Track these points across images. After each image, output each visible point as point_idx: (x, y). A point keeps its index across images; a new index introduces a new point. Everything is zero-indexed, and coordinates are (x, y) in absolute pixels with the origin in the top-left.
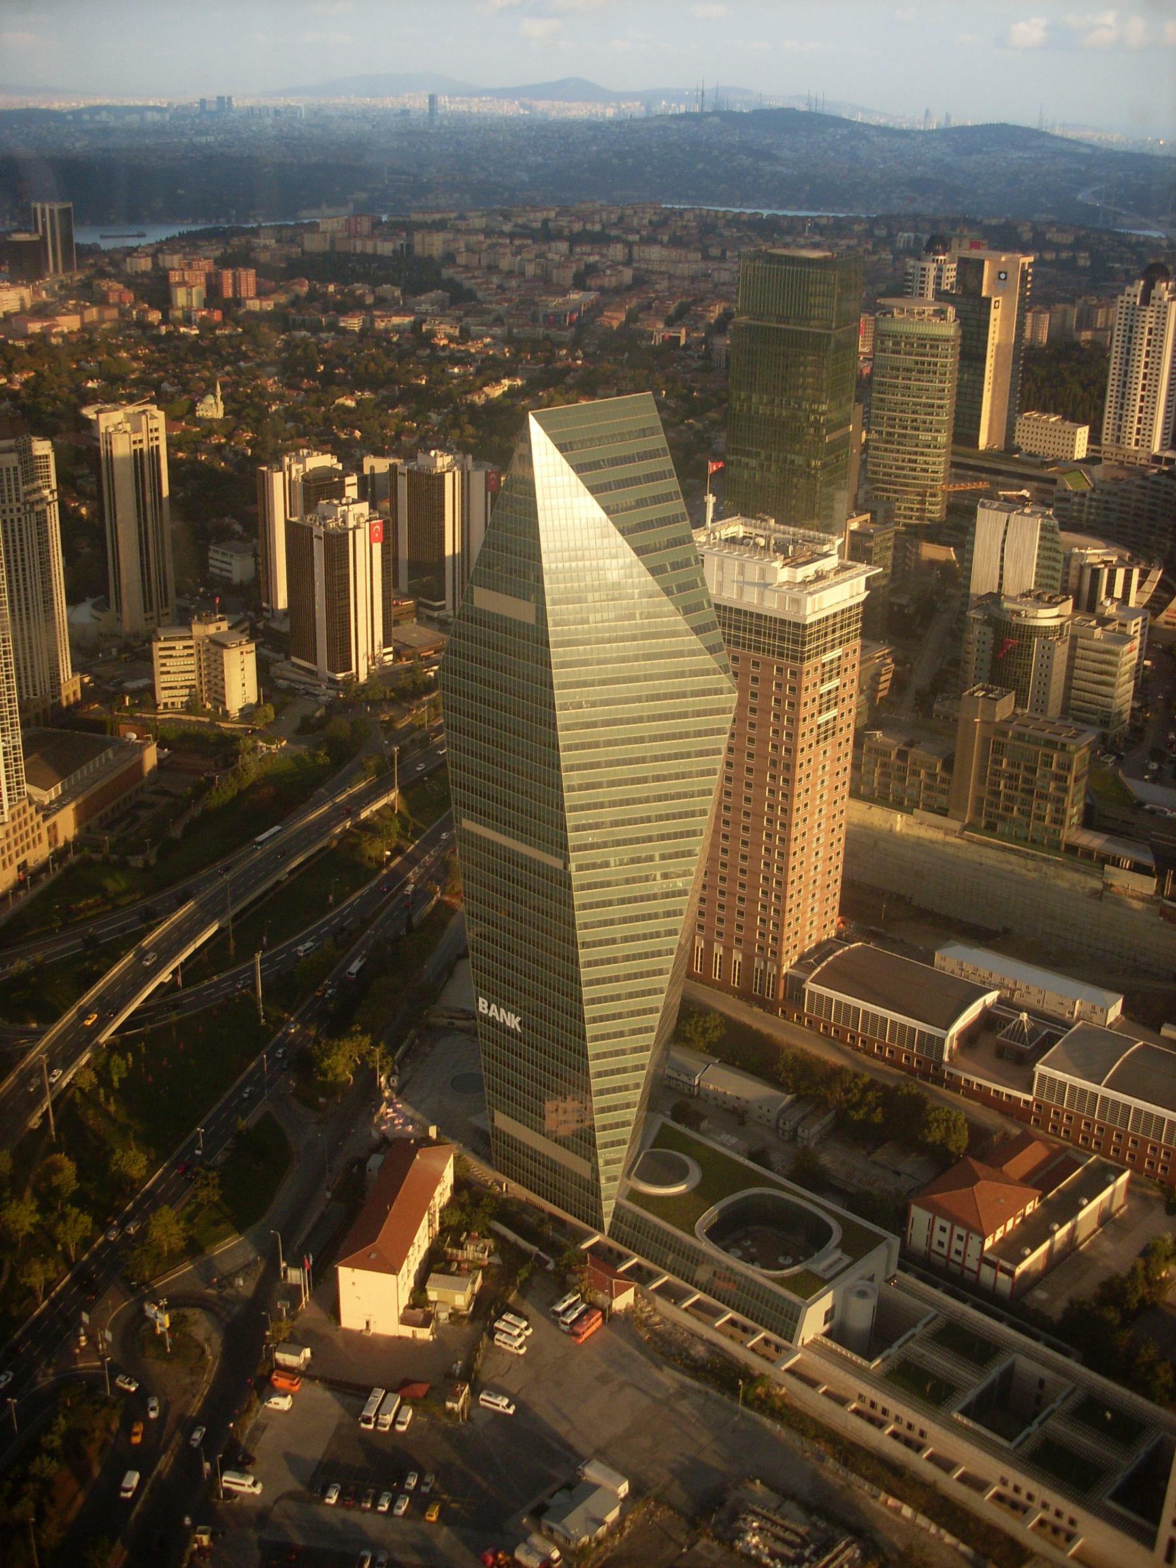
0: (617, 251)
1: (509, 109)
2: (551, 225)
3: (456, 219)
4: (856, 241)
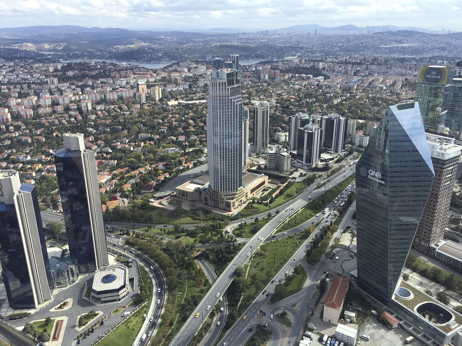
0: (364, 66)
1: (336, 32)
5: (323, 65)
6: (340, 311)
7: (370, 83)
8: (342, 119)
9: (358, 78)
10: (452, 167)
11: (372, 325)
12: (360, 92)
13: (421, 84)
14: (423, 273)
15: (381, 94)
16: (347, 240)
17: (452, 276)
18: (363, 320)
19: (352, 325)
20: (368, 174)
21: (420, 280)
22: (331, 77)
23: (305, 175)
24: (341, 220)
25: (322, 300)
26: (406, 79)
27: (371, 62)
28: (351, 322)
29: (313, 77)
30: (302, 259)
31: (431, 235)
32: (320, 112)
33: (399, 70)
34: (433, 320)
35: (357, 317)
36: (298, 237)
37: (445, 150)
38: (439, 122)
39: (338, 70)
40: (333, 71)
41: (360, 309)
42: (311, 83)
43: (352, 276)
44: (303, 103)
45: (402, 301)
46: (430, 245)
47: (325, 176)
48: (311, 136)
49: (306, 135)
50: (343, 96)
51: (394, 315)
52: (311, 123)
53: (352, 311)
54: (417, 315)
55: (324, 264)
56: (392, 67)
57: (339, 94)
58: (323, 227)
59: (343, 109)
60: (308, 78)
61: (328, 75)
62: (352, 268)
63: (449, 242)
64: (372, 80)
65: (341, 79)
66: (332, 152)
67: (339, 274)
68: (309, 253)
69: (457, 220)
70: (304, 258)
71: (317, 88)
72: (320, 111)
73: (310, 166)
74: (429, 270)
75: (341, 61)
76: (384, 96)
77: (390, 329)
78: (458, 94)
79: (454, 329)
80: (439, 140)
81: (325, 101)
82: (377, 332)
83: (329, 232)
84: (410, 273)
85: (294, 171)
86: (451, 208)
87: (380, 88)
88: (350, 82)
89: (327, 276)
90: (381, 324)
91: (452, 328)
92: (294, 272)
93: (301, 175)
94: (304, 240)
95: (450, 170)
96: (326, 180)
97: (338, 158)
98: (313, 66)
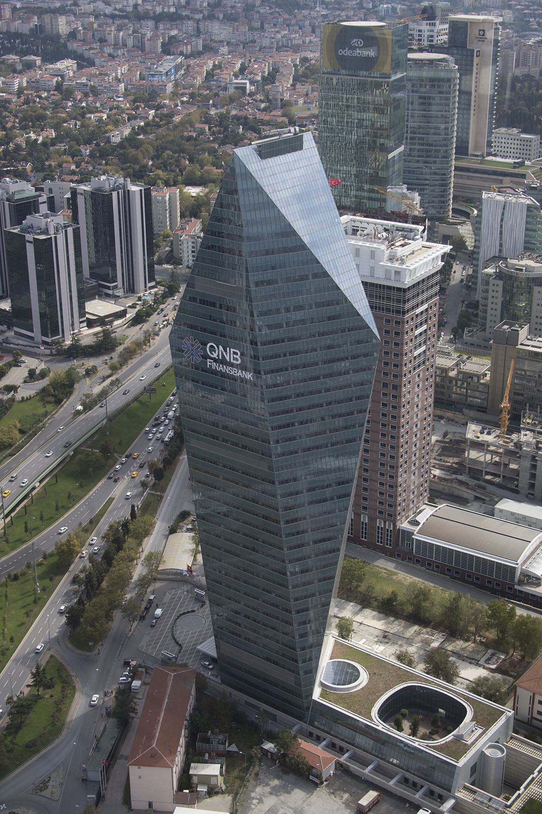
0: (189, 25)
2: (139, 8)
3: (71, 5)
4: (352, 13)
5: (68, 23)
6: (177, 769)
7: (210, 75)
8: (134, 189)
9: (174, 60)
10: (425, 306)
11: (268, 785)
12: (182, 102)
13: (330, 76)
14: (388, 608)
15: (242, 106)
16: (182, 553)
17: (456, 600)
18: (242, 779)
19: (216, 799)
20: (206, 357)
21: (382, 627)
22: (97, 61)
23: (43, 375)
24: (162, 497)
25: (125, 750)
26: (304, 60)
27: (206, 13)
28: (212, 792)
29: (43, 61)
30: (57, 640)
31: (396, 499)
32: (73, 173)
33: (283, 33)
34: (422, 730)
35: (226, 773)
36: (39, 571)
37: (402, 261)
38: (384, 182)
39: (116, 38)
40: (102, 41)
41: (233, 748)
42: (37, 82)
43: (205, 656)
44: (18, 148)
45: (343, 699)
46: (398, 524)
47: (104, 370)
48: (45, 250)
49: (30, 250)
50: (135, 118)
51: (324, 743)
52: (44, 208)
53: (212, 761)
54: (380, 728)
55: (121, 640)
56: (266, 26)
57: (123, 111)
58: (111, 527)
59: (140, 157)
60: (29, 66)
61: (87, 54)
62: (200, 636)
63: (443, 507)
64: (214, 65)
65: (126, 67)
66: (120, 293)
67: (166, 662)
68: (73, 617)
69: (458, 442)
70: (62, 634)
71: (58, 97)
72: (73, 167)
73: (57, 343)
74: (400, 598)
75: (120, 10)
76: (250, 111)
77: (316, 785)
78: (429, 98)
79: (473, 743)
80: (385, 234)
81: (86, 137)
82: (283, 803)
83: (130, 540)
84: (356, 613)
85: (10, 365)
86: (438, 412)
87: (236, 88)
88: (153, 75)
89: (134, 675)
90: (292, 777)
91: (469, 743)
92: (35, 685)
93: (32, 376)
94: (57, 578)
95: (422, 313)
96: (108, 381)
97: (138, 308)
98: (39, 29)
